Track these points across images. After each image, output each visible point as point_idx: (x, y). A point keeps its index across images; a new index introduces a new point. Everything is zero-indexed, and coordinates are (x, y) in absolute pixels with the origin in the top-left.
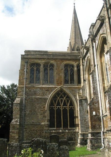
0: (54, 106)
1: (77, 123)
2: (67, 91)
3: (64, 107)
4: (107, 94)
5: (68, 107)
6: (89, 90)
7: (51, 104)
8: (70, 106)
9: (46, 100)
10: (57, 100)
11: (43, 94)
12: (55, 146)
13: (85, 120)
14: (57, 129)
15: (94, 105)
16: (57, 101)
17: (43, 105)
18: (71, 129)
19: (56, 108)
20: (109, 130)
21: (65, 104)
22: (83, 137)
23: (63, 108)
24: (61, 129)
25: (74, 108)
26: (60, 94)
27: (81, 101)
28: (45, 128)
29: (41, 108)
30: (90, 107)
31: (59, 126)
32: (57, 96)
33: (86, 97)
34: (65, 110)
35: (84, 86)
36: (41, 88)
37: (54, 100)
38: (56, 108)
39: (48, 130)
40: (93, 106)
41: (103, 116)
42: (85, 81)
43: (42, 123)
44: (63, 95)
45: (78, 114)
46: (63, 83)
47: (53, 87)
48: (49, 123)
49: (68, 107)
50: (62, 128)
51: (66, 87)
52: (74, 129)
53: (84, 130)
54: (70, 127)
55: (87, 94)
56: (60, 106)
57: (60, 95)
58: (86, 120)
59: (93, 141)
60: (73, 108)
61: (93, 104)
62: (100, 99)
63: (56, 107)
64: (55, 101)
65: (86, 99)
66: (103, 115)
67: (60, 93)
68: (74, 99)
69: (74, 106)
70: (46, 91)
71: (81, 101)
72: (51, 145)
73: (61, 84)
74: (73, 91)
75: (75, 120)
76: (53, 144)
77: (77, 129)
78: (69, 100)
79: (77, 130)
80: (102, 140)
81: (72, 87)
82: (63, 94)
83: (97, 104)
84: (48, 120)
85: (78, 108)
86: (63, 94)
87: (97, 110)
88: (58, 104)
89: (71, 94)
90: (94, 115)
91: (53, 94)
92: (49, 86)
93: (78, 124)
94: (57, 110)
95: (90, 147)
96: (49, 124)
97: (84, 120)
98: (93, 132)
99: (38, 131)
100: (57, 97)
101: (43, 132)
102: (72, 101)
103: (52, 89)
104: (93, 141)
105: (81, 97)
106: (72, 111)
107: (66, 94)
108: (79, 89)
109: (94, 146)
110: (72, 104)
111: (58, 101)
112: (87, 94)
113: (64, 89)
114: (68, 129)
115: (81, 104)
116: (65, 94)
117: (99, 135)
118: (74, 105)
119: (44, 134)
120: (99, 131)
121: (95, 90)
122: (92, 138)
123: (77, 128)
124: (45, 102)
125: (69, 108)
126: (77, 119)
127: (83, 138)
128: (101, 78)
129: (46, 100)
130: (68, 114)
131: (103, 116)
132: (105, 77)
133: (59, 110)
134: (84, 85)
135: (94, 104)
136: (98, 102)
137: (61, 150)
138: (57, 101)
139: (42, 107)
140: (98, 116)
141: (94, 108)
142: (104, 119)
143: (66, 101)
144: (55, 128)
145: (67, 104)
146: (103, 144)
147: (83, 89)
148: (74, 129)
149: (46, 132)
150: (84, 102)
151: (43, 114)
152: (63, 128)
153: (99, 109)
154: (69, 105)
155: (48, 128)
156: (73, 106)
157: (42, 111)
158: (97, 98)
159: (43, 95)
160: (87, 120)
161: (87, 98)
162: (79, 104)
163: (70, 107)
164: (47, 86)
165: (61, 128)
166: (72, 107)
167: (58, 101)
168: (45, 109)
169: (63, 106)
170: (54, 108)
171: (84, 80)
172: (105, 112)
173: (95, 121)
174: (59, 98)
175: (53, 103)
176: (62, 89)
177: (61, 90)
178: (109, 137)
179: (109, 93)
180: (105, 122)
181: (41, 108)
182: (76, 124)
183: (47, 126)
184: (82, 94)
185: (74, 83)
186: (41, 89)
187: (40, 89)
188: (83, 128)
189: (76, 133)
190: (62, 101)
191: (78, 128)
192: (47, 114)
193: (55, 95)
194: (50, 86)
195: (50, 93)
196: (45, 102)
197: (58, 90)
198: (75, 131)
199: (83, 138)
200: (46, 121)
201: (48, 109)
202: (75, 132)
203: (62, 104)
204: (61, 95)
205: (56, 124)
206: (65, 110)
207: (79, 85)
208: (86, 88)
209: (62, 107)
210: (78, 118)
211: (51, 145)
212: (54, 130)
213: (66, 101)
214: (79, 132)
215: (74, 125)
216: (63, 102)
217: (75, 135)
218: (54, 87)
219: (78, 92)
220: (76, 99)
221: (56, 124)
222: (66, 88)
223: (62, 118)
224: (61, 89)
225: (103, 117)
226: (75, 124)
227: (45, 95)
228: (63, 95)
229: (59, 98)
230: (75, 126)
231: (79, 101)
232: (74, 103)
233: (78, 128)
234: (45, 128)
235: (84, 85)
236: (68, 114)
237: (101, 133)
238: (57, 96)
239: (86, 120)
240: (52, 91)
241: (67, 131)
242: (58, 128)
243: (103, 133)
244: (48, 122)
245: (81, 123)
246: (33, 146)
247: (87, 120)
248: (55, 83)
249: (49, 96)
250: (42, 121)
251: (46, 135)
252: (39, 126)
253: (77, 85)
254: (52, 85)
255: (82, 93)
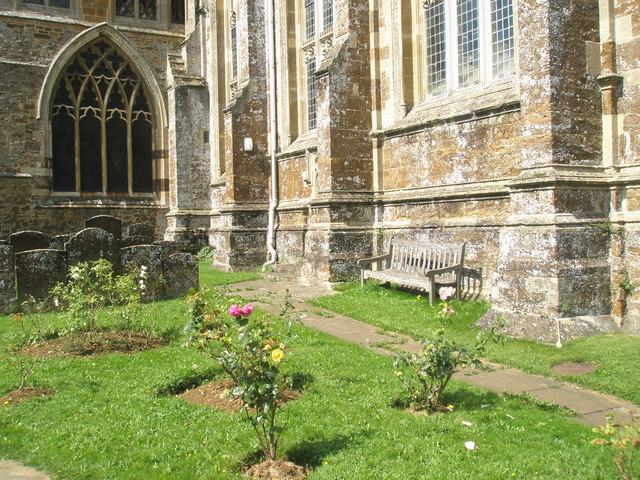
0: (70, 103)
1: (163, 177)
2: (129, 49)
3: (113, 111)
4: (328, 81)
5: (128, 113)
6: (219, 54)
7: (60, 95)
8: (136, 108)
9: (35, 75)
10: (83, 79)
11: (25, 51)
12: (152, 254)
13: (195, 168)
14: (84, 195)
15: (247, 113)
16: (85, 83)
17: (23, 99)
18: (139, 199)
19: (82, 112)
20: (325, 204)
21: (115, 101)
22: (187, 226)
23: (108, 114)
24: (102, 198)
25: (154, 117)
26: (96, 57)
27: (182, 93)
28: (34, 192)
29: (18, 110)
30: (234, 121)
31: (91, 184)
32: (82, 62)
33: (204, 80)
34: (116, 125)
35: (195, 34)
36: (15, 22)
37: (70, 77)
38: (82, 112)
39: (48, 197)
40: (244, 116)
41: (279, 154)
42: (204, 14)
43: (19, 172)
44: (109, 64)
45: (166, 144)
46: (108, 11)
47: (66, 24)
48: (50, 173)
49: (129, 112)
50: (105, 194)
51: (122, 31)
52: (150, 199)
53: (190, 204)
54: (134, 191)
55: (209, 67)
56: (96, 105)
57: (97, 63)
58: (198, 165)
59: (240, 239)
60: (149, 116)
61: (247, 111)
62: (271, 92)
63: (78, 111)
64: (76, 86)
65: (203, 89)
66: (278, 150)
67: (96, 50)
68: (152, 82)
69: (154, 111)
70: (36, 36)
71: (186, 94)
72: (136, 253)
73: (102, 13)
74: (154, 49)
75: (154, 164)
76: (144, 248)
77: (163, 198)
78: (135, 84)
79: (162, 202)
80: (270, 235)
81: (148, 31)
82: (109, 58)
83: (260, 111)
84: (47, 159)
85: (168, 121)
86: (109, 58)
87: (259, 132)
88: (90, 99)
89: (143, 62)
90: (248, 152)
91: (69, 54)
92: (51, 16)
93: (167, 182)
94: (82, 122)
95: (228, 258)
96: (52, 175)
97: (192, 165)
98: (241, 208)
99: (7, 204)
100: (85, 67)
101: (27, 208)
102: (148, 91)
103: (64, 31)
104: (240, 239)
105: (183, 79)
106: (145, 132)
107: (121, 59)
108: (177, 46)
109: (242, 255)
110: (144, 102)
111: (90, 85)
112: (205, 69)
113: (116, 39)
114: (127, 199)
115: (183, 106)
116: (117, 58)
117: (259, 219)
118: (150, 108)
119: (31, 214)
120: (258, 207)
121: (256, 58)
122: (235, 228)
123: (163, 193)
124: (33, 86)
125: (133, 116)
126: (163, 160)
127: (185, 229)
128: (284, 14)
129: (35, 75)
130: (129, 140)
131: (279, 154)
132: (300, 13)
133: (90, 122)
134: (197, 30)
135: (249, 109)
136: (264, 102)
137: (171, 266)
138: (85, 83)
139: (21, 106)
140: (261, 153)
141: (248, 126)
142: (284, 165)
143: (122, 90)
144: (77, 194)
145: (71, 96)
146: (271, 249)
147: (194, 48)
148: (150, 199)
149: (38, 208)
150: (193, 97)
151: (26, 135)
152: (108, 191)
153: (265, 131)
154: (79, 101)
155: (48, 191)
156: (147, 110)
157: (21, 121)
158: (263, 89)
159: (25, 56)
160: (201, 168)
161: (205, 82)
162: (177, 107)
163: (139, 113)
164: (43, 18)
165: (98, 194)
166: (145, 113)
167: (90, 85)
168: (35, 113)
169: (110, 106)
170: (72, 111)
171: (199, 12)
172: (288, 140)
173: (250, 170)
174: (91, 72)
175: (67, 93)
176: (108, 37)
177: (102, 43)
178: (320, 225)
179: (332, 78)
180: (284, 178)
181: (18, 110)
182: (158, 181)
183: (42, 183)
184: (190, 67)
185: (154, 18)
186: (13, 26)
187: (9, 26)
188: (185, 196)
189: (156, 215)
190: (103, 86)
191: (167, 196)
192: (44, 134)
193: (76, 61)
194: (54, 19)
195: (55, 49)
196: (35, 86)
197: (88, 39)
198: (155, 205)
199: (185, 229)
200: (39, 164)
201: (46, 116)
202: (152, 209)
203: (103, 98)
204: (102, 64)
205: (78, 175)
206: (116, 125)
207: (177, 26)
208: (204, 44)
209: (103, 110)
210: (166, 157)
211: (136, 253)
212: (71, 200)
213: (122, 87)
214: (168, 210)
215: (148, 183)
216: (109, 90)
217: (153, 220)
218: (72, 24)
219: (172, 57)
220: (162, 82)
221: (78, 175)
222: (124, 33)
223: (104, 154)
224: (101, 35)
225: (277, 159)
226: (154, 178)
227: (34, 55)
228: (109, 64)
229: (93, 74)
230: (154, 186)
231: (176, 93)
232: (152, 98)
233: (167, 196)
234: (34, 192)
235: (197, 30)
236: (129, 140)
237: (265, 212)
238: (82, 62)
239: (198, 165)
240: (62, 41)
241: (123, 204)
242: (90, 194)
243: (276, 212)
244: (46, 167)
245: (179, 177)
246: (71, 254)
247: (201, 168)
248: (77, 5)
249: (53, 62)
250: (22, 164)
251: (41, 217)
252: (10, 181)
253: (169, 29)
254: (60, 14)
255: (189, 61)
